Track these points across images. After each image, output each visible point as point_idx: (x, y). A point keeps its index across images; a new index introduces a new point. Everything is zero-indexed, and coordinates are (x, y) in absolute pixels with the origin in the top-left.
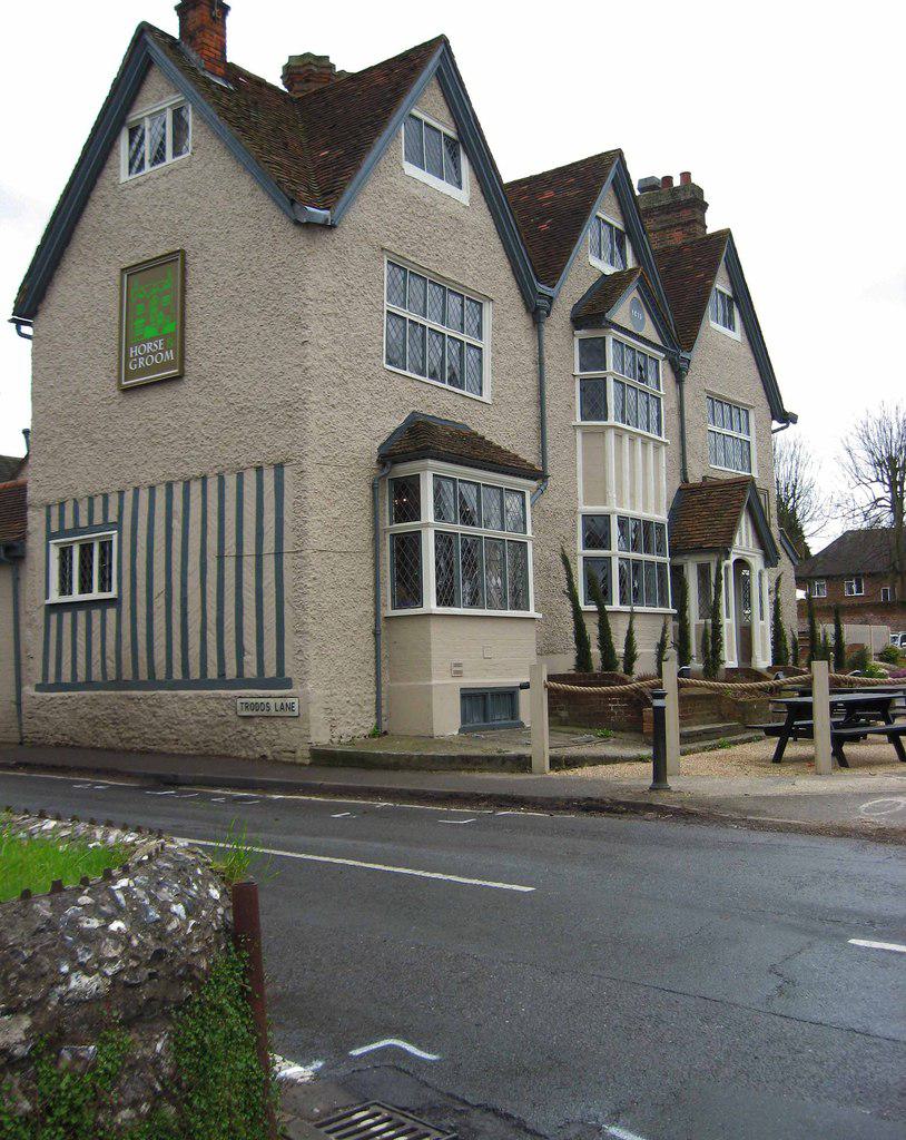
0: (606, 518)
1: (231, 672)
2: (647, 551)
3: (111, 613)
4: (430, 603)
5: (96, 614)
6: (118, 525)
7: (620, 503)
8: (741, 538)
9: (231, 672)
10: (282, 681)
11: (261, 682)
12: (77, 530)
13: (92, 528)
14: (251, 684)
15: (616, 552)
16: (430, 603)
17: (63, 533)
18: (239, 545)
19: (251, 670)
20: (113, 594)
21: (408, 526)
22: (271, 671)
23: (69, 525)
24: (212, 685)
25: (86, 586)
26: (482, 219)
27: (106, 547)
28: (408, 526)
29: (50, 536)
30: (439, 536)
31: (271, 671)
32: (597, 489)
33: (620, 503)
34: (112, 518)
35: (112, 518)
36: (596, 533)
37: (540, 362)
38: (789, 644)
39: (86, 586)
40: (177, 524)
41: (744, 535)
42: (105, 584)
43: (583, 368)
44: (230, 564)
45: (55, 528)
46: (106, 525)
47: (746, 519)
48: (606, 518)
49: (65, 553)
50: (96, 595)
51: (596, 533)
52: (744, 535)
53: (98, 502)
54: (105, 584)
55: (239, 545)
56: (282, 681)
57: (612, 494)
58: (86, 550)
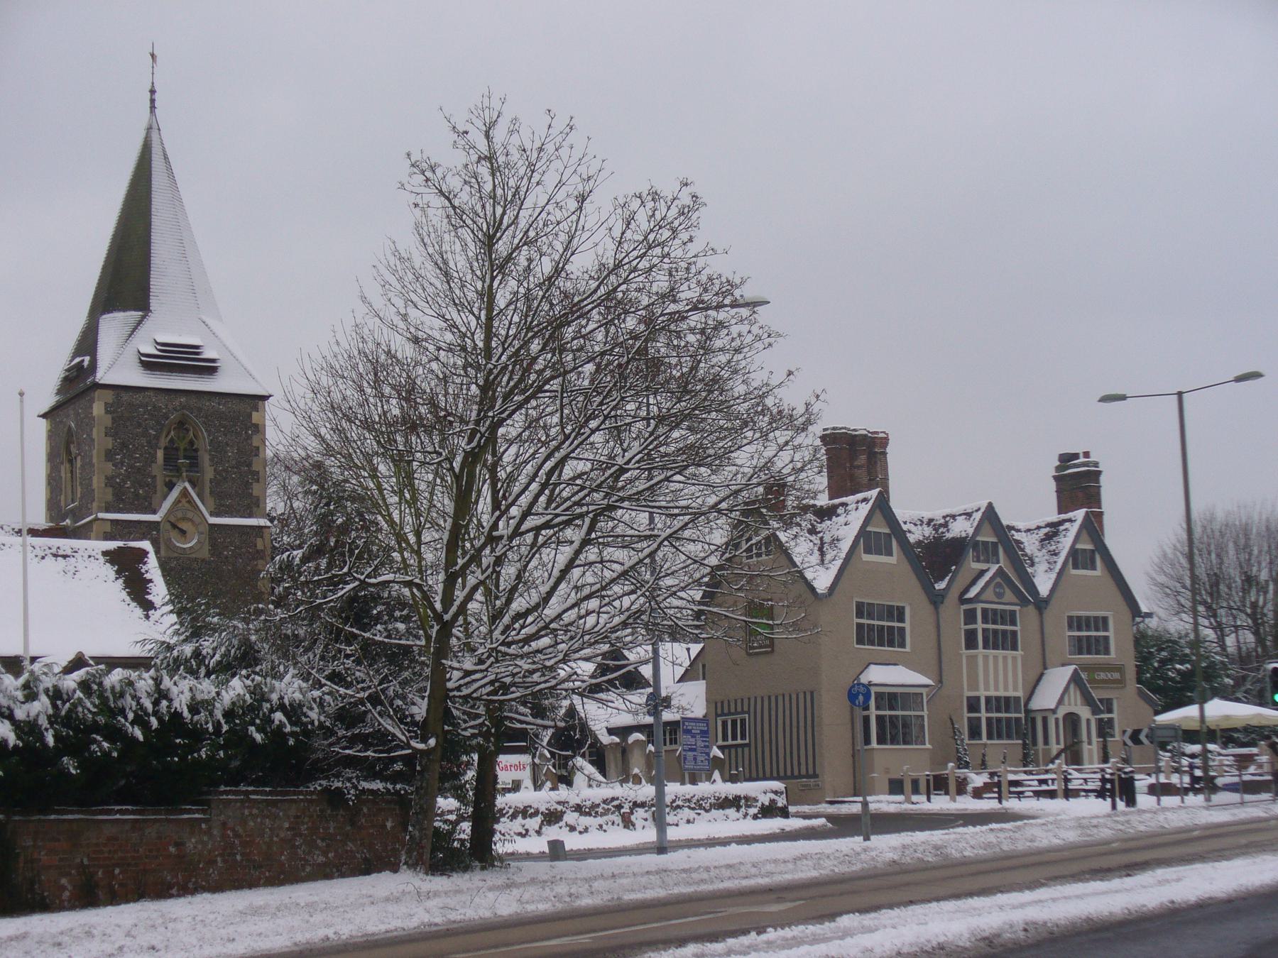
0: (978, 698)
1: (796, 773)
2: (1007, 711)
3: (746, 750)
4: (874, 745)
5: (740, 750)
6: (748, 712)
7: (987, 689)
8: (1069, 699)
9: (796, 773)
10: (815, 776)
11: (808, 776)
12: (730, 713)
13: (736, 713)
14: (804, 777)
15: (983, 715)
16: (874, 745)
17: (723, 714)
18: (798, 722)
19: (803, 772)
20: (747, 741)
21: (866, 713)
22: (811, 772)
23: (726, 711)
24: (796, 778)
25: (734, 738)
26: (906, 567)
27: (743, 721)
28: (866, 713)
29: (717, 715)
30: (878, 717)
31: (811, 772)
32: (974, 684)
33: (987, 689)
34: (746, 709)
35: (746, 709)
36: (973, 705)
37: (938, 627)
38: (204, 797)
39: (734, 738)
40: (773, 713)
41: (1072, 698)
42: (743, 737)
43: (965, 624)
44: (795, 730)
45: (719, 711)
46: (743, 712)
47: (1075, 692)
48: (978, 698)
49: (724, 724)
50: (739, 741)
51: (973, 705)
52: (1072, 698)
53: (739, 702)
54: (743, 737)
55: (798, 722)
56: (815, 776)
57: (982, 686)
58: (734, 722)
